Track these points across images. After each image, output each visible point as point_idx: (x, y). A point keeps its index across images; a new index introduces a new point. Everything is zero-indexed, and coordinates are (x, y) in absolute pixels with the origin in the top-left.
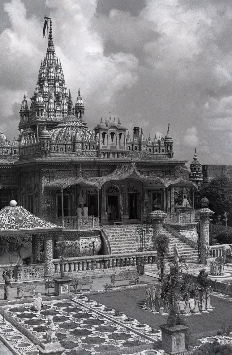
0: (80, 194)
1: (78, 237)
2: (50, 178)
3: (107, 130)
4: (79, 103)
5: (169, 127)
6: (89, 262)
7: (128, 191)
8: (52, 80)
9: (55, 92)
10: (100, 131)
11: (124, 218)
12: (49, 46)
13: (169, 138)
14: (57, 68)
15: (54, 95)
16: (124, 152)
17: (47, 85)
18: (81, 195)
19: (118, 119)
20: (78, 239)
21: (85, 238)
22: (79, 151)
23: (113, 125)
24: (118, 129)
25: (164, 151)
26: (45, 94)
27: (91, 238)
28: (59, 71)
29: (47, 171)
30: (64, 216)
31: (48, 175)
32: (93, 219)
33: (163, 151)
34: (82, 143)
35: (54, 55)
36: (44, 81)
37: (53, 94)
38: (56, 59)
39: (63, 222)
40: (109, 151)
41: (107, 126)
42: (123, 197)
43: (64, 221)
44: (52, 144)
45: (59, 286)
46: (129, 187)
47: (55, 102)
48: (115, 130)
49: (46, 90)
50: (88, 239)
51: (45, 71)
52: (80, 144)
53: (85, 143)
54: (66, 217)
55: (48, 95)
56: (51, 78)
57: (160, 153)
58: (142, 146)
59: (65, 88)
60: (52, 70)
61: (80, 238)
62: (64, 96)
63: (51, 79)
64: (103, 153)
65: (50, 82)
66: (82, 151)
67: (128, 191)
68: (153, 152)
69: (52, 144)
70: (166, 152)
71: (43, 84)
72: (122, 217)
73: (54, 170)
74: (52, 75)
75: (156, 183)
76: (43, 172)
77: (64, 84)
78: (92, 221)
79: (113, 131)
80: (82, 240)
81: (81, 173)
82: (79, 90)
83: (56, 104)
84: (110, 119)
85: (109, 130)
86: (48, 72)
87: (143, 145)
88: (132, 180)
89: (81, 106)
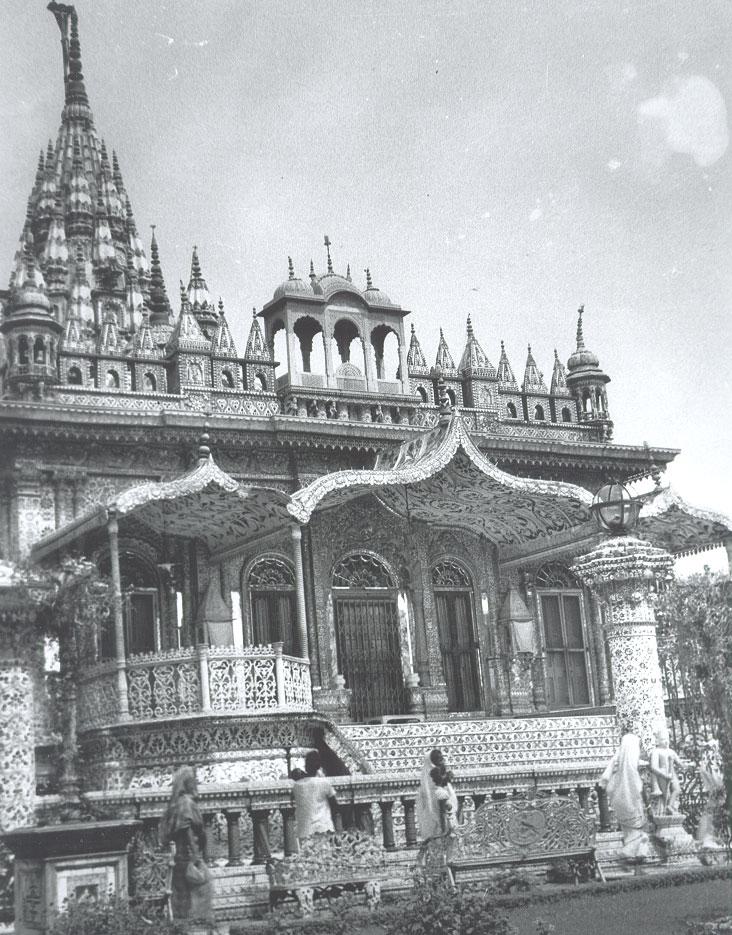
0: (207, 587)
1: (206, 752)
2: (57, 507)
3: (319, 305)
4: (196, 303)
5: (580, 321)
6: (266, 812)
7: (434, 582)
8: (86, 216)
9: (95, 263)
10: (289, 312)
11: (424, 703)
12: (69, 101)
13: (586, 364)
14: (101, 175)
15: (94, 272)
16: (402, 405)
17: (63, 237)
18: (215, 587)
19: (366, 273)
20: (206, 763)
21: (240, 754)
22: (196, 393)
23: (342, 289)
24: (366, 304)
25: (574, 417)
26: (54, 266)
27: (273, 758)
28: (111, 186)
29: (44, 472)
30: (127, 656)
31: (51, 496)
32: (280, 662)
33: (566, 412)
34: (212, 358)
35: (93, 133)
36: (48, 222)
37: (89, 267)
38: (99, 147)
39: (123, 684)
40: (336, 395)
41: (317, 290)
42: (416, 604)
43: (129, 682)
44: (68, 355)
45: (40, 873)
46: (436, 561)
47: (95, 296)
48: (356, 310)
49: (58, 251)
50: (257, 763)
51: (51, 187)
52: (198, 359)
53: (226, 360)
54: (135, 660)
55: (66, 273)
56: (80, 210)
57: (554, 420)
58: (478, 388)
59: (137, 250)
60: (81, 181)
61: (217, 755)
62: (135, 280)
63: (79, 213)
64: (308, 403)
65: (74, 225)
66: (214, 393)
67: (434, 582)
68: (526, 418)
69: (68, 355)
70: (579, 419)
71: (46, 234)
72: (417, 698)
73: (74, 469)
74: (84, 198)
75: (561, 528)
76: (21, 479)
77: (134, 237)
78: (274, 671)
79: (347, 316)
80: (225, 765)
81: (207, 448)
82: (194, 253)
83: (100, 304)
84: (330, 268)
85: (331, 307)
86: (66, 189)
87: (481, 385)
88: (445, 532)
89: (205, 313)
